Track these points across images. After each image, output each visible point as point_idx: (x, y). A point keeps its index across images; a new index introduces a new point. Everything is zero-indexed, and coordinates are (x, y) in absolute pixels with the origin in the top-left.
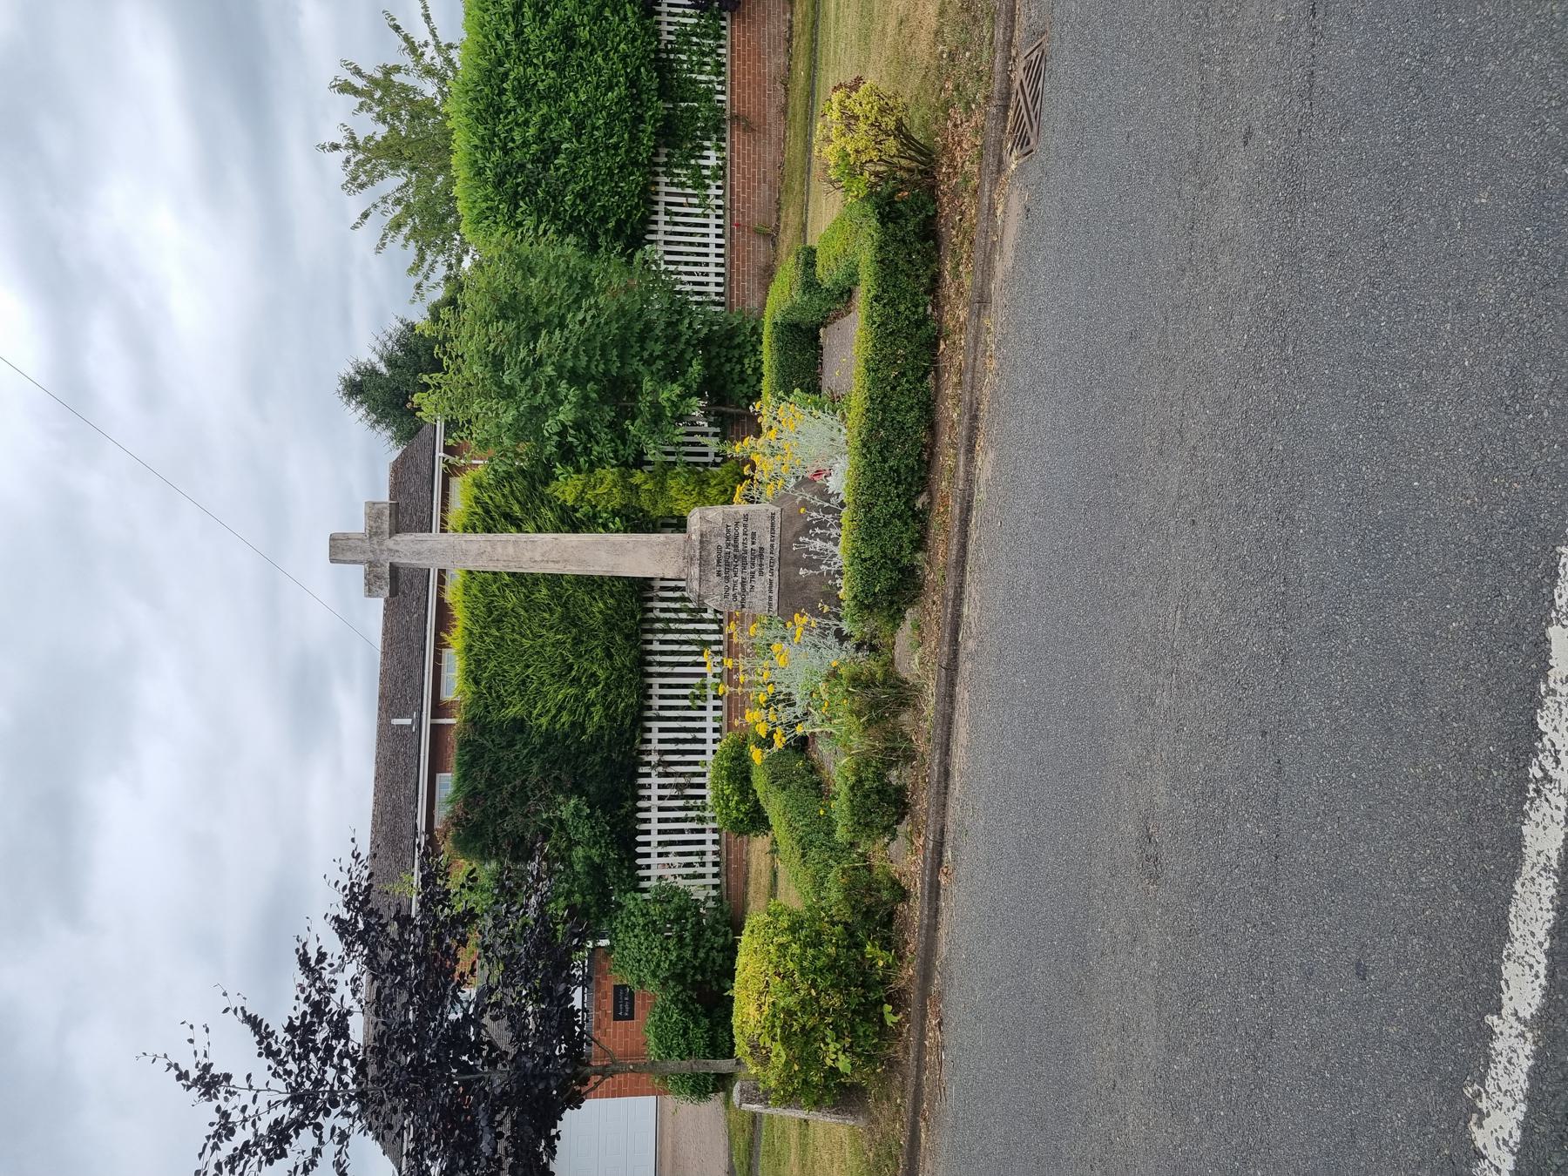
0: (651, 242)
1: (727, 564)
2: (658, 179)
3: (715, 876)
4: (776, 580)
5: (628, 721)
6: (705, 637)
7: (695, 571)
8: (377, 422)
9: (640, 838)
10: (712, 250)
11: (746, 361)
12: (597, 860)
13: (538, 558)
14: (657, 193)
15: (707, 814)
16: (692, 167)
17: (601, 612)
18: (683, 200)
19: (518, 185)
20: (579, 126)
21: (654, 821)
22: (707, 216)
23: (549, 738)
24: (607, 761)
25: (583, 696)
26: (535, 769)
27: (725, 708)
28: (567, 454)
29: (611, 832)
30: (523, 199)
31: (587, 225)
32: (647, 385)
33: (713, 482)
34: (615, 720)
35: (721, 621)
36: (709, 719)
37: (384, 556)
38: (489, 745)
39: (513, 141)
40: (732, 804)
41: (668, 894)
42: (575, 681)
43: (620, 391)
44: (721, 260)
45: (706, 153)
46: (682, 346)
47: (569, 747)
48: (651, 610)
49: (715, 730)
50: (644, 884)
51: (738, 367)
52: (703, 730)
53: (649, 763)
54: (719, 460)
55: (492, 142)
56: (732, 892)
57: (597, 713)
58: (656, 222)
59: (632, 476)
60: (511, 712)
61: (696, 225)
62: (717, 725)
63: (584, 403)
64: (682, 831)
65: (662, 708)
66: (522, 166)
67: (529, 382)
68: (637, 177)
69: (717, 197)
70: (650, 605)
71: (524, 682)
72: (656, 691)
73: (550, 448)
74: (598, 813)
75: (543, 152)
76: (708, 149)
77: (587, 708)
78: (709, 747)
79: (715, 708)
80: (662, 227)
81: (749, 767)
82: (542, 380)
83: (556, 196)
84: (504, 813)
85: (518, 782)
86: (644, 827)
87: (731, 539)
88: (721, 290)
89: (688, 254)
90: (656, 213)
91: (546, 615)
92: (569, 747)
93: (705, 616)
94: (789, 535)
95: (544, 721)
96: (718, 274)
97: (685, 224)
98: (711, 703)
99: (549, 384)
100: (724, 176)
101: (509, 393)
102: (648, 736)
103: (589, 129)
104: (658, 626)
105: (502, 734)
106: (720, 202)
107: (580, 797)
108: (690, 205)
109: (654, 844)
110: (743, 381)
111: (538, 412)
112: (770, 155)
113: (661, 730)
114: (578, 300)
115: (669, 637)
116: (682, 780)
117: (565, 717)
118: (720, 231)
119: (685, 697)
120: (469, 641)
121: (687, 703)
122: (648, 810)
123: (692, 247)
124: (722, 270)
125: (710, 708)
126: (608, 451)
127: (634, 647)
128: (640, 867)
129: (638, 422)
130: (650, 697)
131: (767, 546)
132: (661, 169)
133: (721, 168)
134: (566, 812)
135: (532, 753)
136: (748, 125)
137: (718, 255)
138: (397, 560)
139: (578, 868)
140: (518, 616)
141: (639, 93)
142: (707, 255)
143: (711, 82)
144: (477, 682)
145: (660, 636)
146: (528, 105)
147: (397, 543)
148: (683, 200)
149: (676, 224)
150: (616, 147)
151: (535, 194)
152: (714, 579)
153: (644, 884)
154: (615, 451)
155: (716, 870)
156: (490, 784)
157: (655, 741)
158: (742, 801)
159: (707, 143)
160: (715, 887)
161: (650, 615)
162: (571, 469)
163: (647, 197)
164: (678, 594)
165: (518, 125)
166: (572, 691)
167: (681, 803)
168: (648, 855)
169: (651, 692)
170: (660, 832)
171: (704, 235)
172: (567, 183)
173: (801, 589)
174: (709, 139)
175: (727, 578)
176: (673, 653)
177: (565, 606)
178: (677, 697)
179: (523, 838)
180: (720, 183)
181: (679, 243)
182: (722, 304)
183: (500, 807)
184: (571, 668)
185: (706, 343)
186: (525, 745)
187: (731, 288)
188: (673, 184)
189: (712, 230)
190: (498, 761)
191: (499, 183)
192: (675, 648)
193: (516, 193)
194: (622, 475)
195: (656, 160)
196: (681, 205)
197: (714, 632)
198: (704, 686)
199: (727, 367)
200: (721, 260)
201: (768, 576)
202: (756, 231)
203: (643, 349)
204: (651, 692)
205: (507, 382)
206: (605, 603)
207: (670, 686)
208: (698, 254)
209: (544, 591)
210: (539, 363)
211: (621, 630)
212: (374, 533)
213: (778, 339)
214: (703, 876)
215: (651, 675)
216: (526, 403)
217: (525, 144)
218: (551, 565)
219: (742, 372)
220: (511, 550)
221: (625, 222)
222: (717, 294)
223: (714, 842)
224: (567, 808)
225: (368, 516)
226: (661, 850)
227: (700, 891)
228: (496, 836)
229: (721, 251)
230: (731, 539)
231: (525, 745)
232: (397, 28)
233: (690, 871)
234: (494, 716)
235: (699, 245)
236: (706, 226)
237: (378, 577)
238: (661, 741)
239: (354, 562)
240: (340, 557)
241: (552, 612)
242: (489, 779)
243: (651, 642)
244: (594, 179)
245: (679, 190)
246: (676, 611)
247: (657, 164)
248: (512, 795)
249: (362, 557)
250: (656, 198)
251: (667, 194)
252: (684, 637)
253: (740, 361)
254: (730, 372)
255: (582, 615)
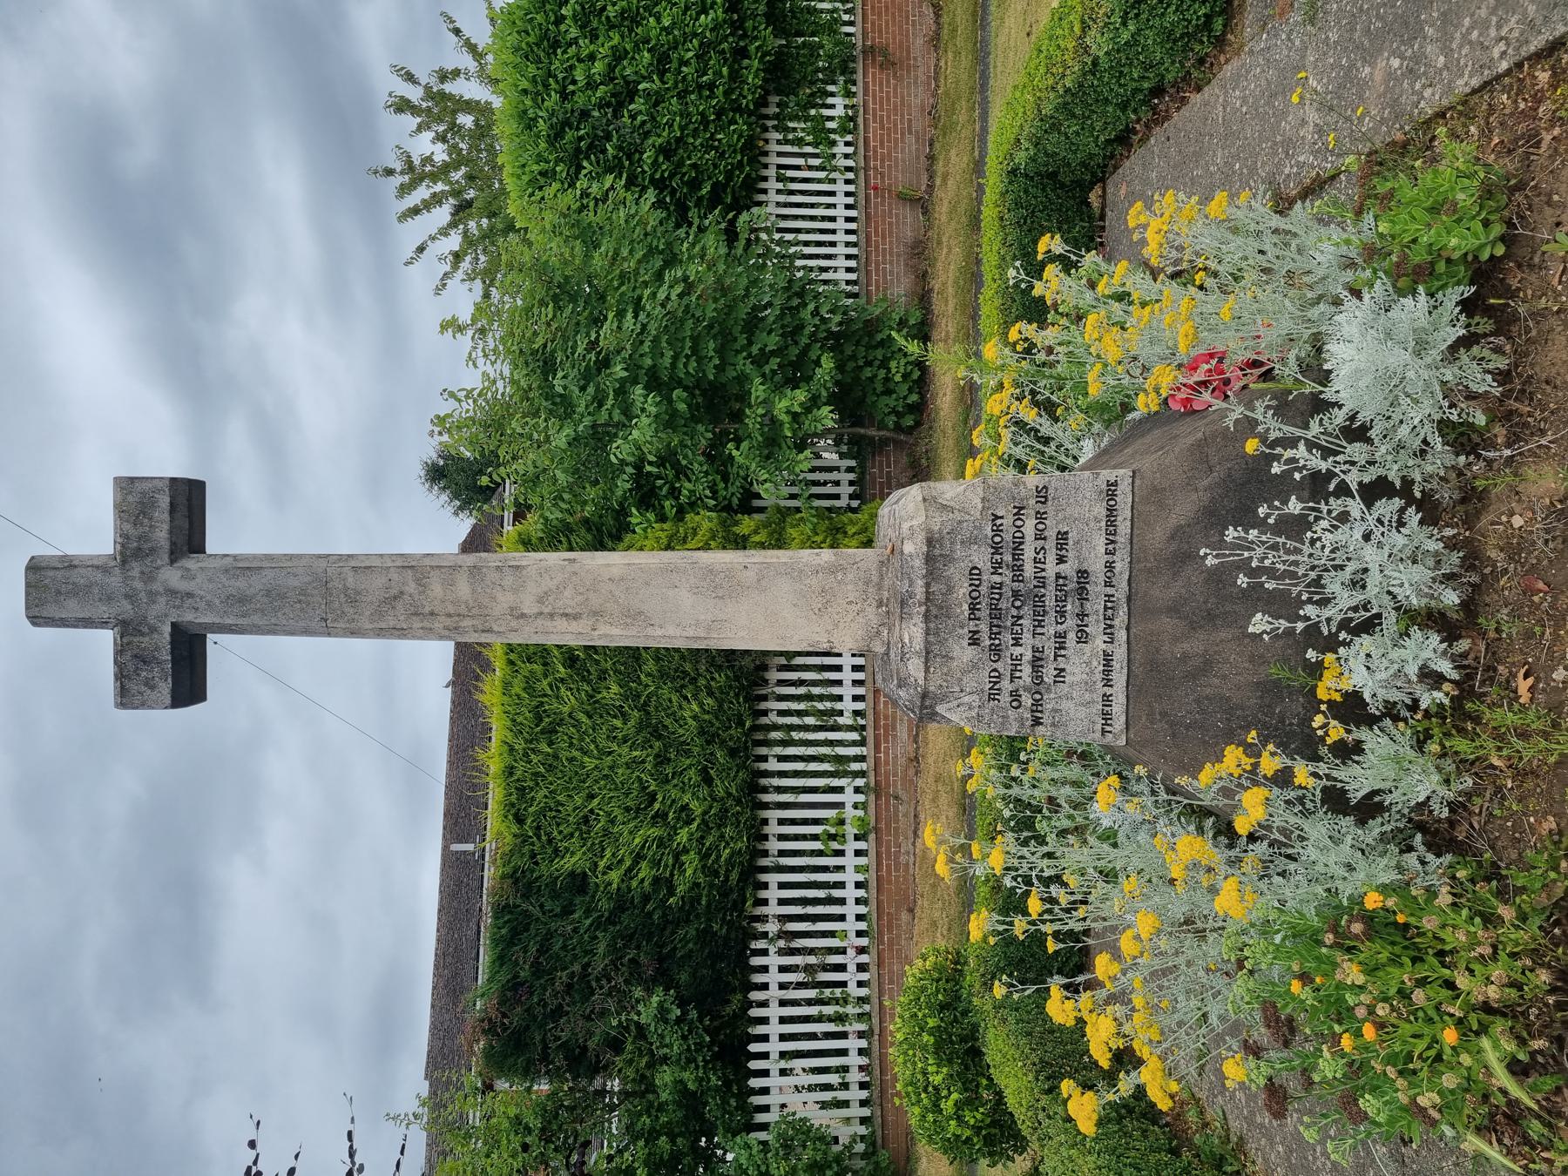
0: (759, 204)
1: (996, 613)
2: (767, 135)
3: (863, 1103)
4: (1120, 654)
5: (734, 876)
6: (841, 751)
7: (913, 633)
8: (461, 508)
9: (754, 1048)
10: (841, 225)
11: (893, 364)
12: (691, 1086)
13: (529, 607)
14: (766, 154)
15: (851, 1010)
16: (813, 119)
17: (695, 718)
18: (800, 161)
19: (581, 139)
20: (662, 63)
21: (774, 1021)
22: (834, 181)
23: (622, 902)
24: (705, 936)
25: (671, 838)
26: (601, 948)
27: (872, 853)
28: (646, 495)
29: (712, 1042)
30: (588, 158)
31: (673, 192)
32: (758, 390)
33: (851, 530)
34: (716, 874)
35: (863, 728)
36: (850, 869)
37: (161, 604)
38: (536, 912)
39: (574, 82)
40: (948, 1106)
41: (799, 1133)
42: (661, 816)
43: (718, 404)
44: (853, 238)
45: (830, 100)
46: (804, 341)
47: (650, 915)
48: (765, 713)
49: (858, 885)
50: (761, 1118)
51: (882, 373)
52: (841, 885)
53: (765, 935)
54: (855, 504)
55: (546, 86)
56: (890, 1132)
57: (691, 862)
58: (765, 191)
59: (737, 523)
60: (569, 863)
61: (819, 193)
62: (860, 878)
63: (668, 421)
64: (812, 1036)
65: (782, 853)
66: (585, 114)
67: (591, 390)
68: (741, 125)
69: (846, 156)
70: (763, 706)
71: (586, 820)
72: (773, 829)
73: (623, 484)
74: (694, 1014)
75: (613, 95)
76: (832, 95)
77: (677, 856)
78: (851, 910)
79: (858, 853)
80: (773, 197)
81: (975, 1028)
82: (610, 386)
83: (631, 152)
84: (558, 1013)
85: (577, 968)
86: (760, 1030)
87: (1006, 550)
88: (853, 276)
89: (808, 231)
90: (765, 179)
91: (618, 723)
92: (650, 915)
93: (841, 720)
94: (1157, 536)
95: (615, 876)
96: (848, 257)
97: (803, 193)
98: (851, 846)
99: (617, 393)
100: (856, 127)
101: (563, 407)
102: (763, 894)
103: (674, 65)
104: (775, 735)
105: (555, 895)
106: (850, 163)
107: (667, 989)
108: (810, 168)
109: (774, 1056)
110: (888, 392)
111: (600, 437)
112: (917, 97)
113: (782, 886)
114: (659, 276)
115: (791, 751)
116: (812, 960)
117: (645, 871)
118: (850, 200)
119: (815, 837)
120: (509, 760)
121: (817, 845)
122: (764, 1004)
123: (818, 219)
124: (854, 251)
125: (850, 853)
126: (702, 489)
127: (743, 766)
128: (750, 1004)
129: (745, 445)
130: (766, 838)
131: (1097, 567)
132: (770, 123)
133: (851, 119)
134: (646, 1014)
135: (597, 925)
136: (884, 58)
137: (848, 232)
138: (189, 617)
139: (664, 1096)
140: (577, 725)
141: (742, 20)
142: (834, 232)
143: (835, 10)
144: (520, 820)
145: (778, 750)
146: (594, 37)
147: (188, 575)
148: (800, 161)
149: (792, 192)
150: (711, 86)
151: (604, 151)
152: (963, 653)
153: (761, 1118)
154: (714, 492)
155: (864, 1094)
156: (537, 970)
157: (773, 902)
158: (971, 1102)
159: (831, 88)
160: (864, 1121)
161: (764, 720)
162: (651, 516)
163: (754, 152)
164: (802, 690)
165: (580, 60)
166: (655, 832)
167: (811, 994)
168: (765, 1073)
169: (767, 830)
170: (783, 1020)
171: (829, 206)
172: (647, 135)
173: (1193, 676)
174: (834, 83)
175: (996, 651)
176: (796, 774)
177: (644, 708)
178: (804, 837)
179: (585, 1049)
180: (849, 138)
181: (796, 217)
182: (855, 296)
183: (552, 1004)
184: (652, 798)
185: (835, 342)
186: (588, 913)
187: (868, 273)
188: (787, 142)
189: (840, 200)
190: (550, 935)
191: (556, 135)
192: (800, 766)
193: (578, 150)
194: (723, 523)
195: (765, 111)
196: (798, 168)
197: (854, 743)
198: (842, 822)
199: (868, 372)
200: (853, 238)
201: (1099, 643)
202: (902, 197)
203: (750, 343)
204: (767, 830)
205: (559, 390)
206: (701, 705)
207: (793, 822)
208: (822, 231)
209: (615, 688)
210: (604, 363)
211: (723, 742)
212: (131, 550)
213: (1018, 204)
214: (845, 1104)
215: (766, 806)
216: (587, 421)
217: (591, 85)
218: (561, 624)
219: (887, 379)
220: (463, 589)
221: (726, 185)
222: (848, 282)
223: (861, 1052)
224: (649, 1007)
225: (121, 510)
226: (783, 1064)
227: (844, 1127)
228: (545, 1047)
229: (853, 226)
230: (1006, 550)
231: (588, 913)
232: (457, 32)
233: (827, 1096)
234: (544, 869)
235: (824, 219)
236: (832, 194)
237: (143, 659)
238: (782, 902)
239: (87, 623)
240: (51, 611)
241: (625, 717)
242: (536, 964)
243: (764, 759)
244: (682, 129)
245: (796, 149)
246: (799, 713)
247: (767, 117)
248: (569, 986)
249: (103, 611)
250: (764, 160)
251: (780, 154)
252: (811, 751)
253: (884, 364)
254: (871, 379)
255: (667, 722)
